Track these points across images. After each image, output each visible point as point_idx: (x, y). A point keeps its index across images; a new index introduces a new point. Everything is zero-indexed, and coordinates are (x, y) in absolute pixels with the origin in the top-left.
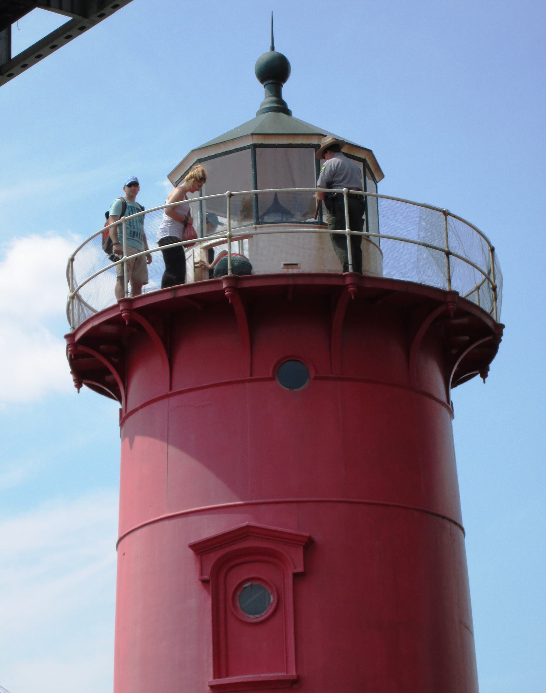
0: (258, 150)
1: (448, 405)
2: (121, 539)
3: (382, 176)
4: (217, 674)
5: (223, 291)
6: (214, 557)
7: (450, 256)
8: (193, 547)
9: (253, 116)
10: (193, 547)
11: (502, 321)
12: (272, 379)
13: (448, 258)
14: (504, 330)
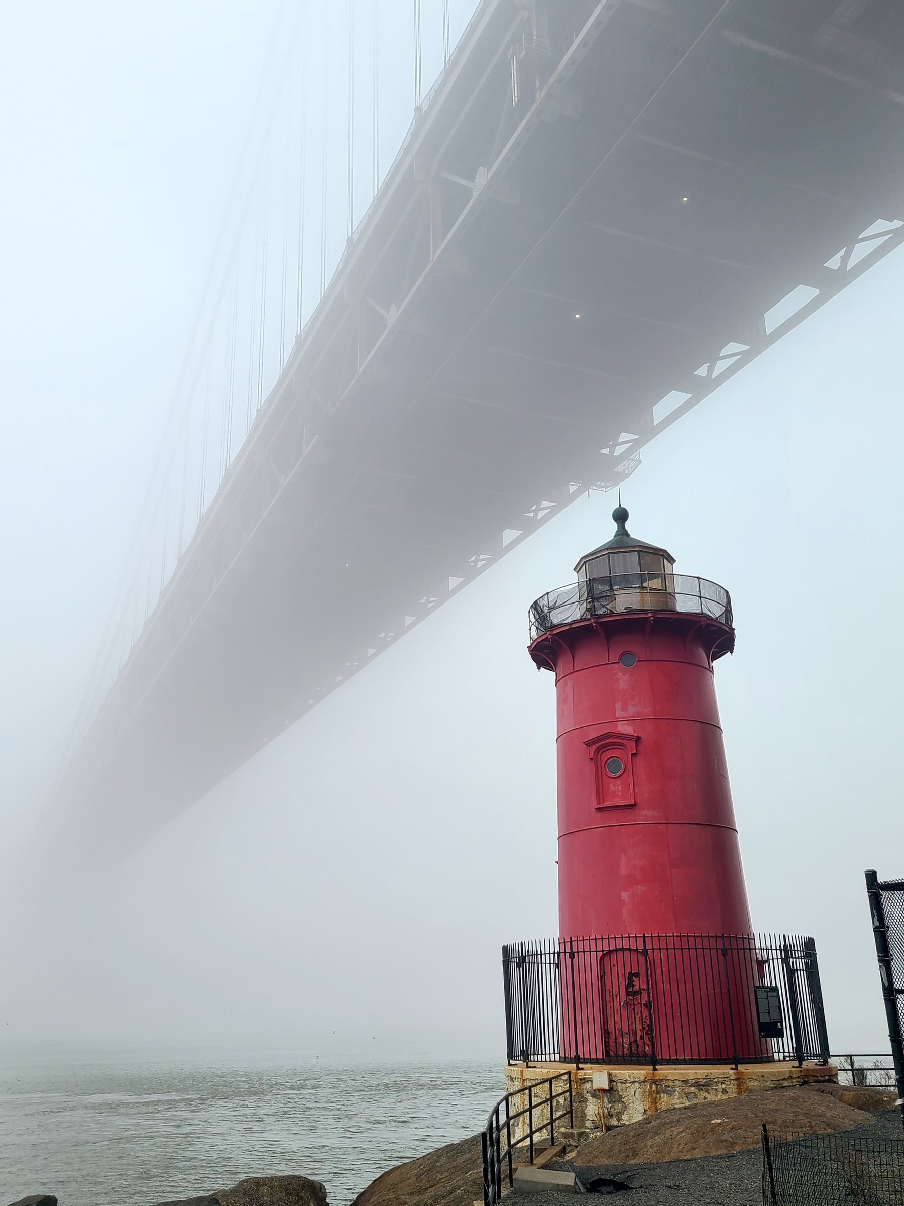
3: (675, 561)
4: (598, 802)
6: (594, 747)
9: (613, 538)
11: (734, 627)
12: (618, 663)
13: (700, 599)
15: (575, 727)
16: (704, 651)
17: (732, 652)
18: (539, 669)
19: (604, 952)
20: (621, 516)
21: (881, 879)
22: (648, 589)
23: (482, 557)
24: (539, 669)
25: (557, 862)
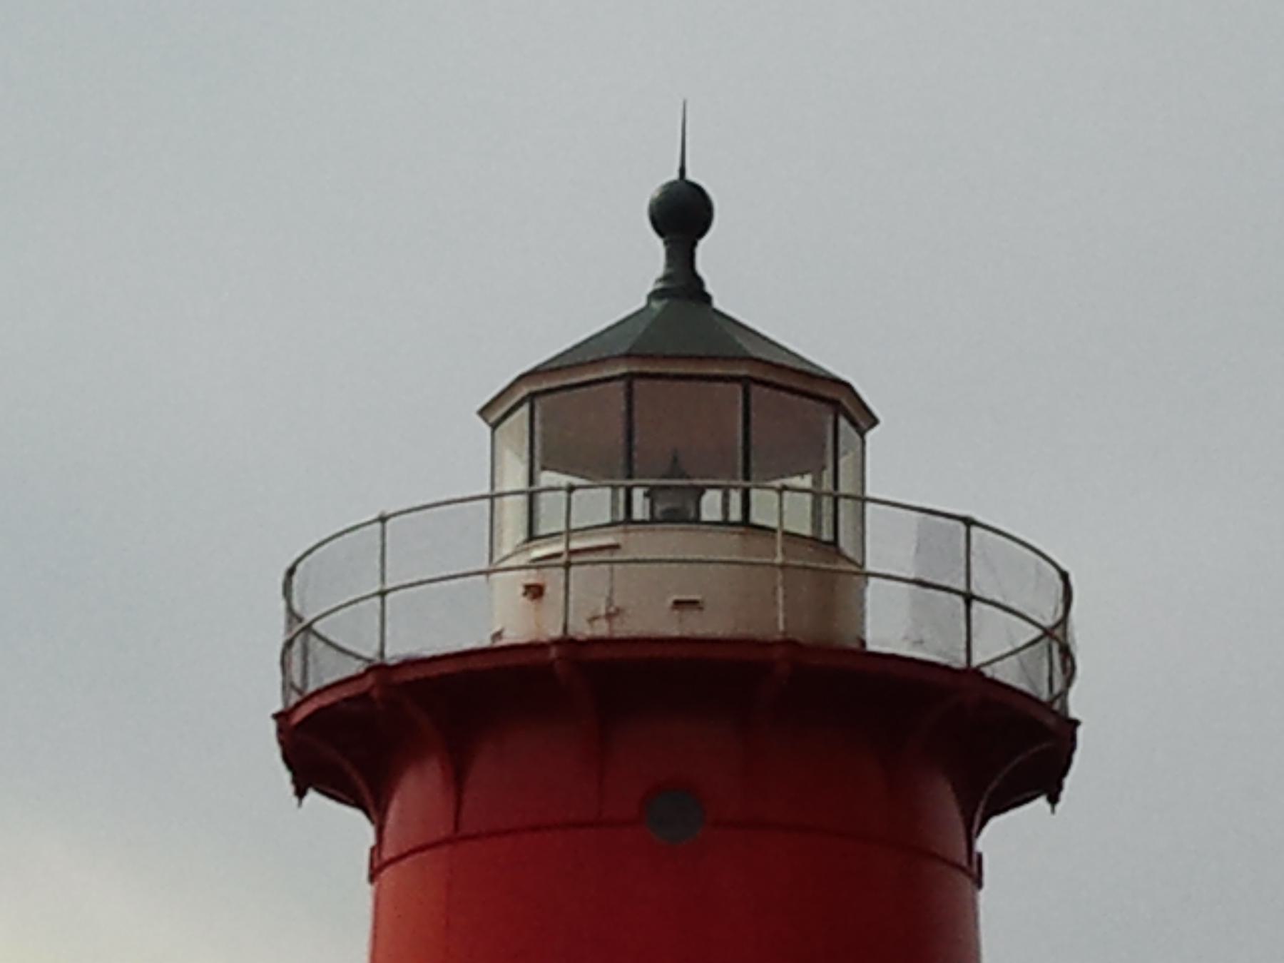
0: (639, 385)
3: (874, 422)
7: (976, 605)
11: (1074, 713)
14: (1081, 732)
16: (955, 790)
18: (300, 793)
22: (779, 535)
24: (300, 793)
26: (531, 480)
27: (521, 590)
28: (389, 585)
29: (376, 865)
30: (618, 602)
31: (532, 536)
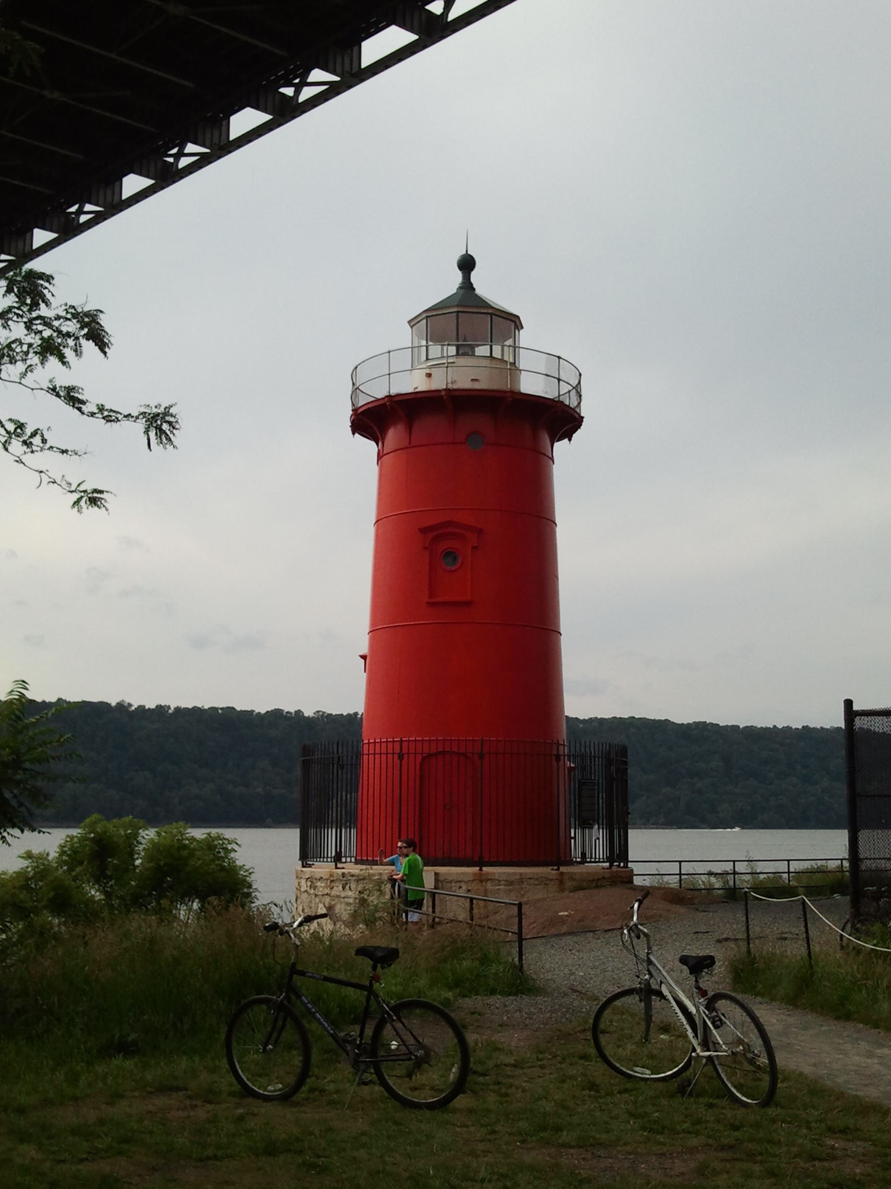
0: (460, 314)
1: (872, 943)
2: (376, 522)
3: (522, 328)
4: (431, 596)
5: (442, 396)
7: (561, 382)
8: (420, 530)
10: (420, 530)
11: (582, 415)
14: (584, 420)
15: (407, 510)
17: (570, 440)
18: (354, 434)
19: (424, 755)
20: (467, 264)
21: (856, 707)
23: (88, 207)
25: (364, 657)
26: (427, 343)
27: (425, 375)
28: (391, 372)
29: (381, 455)
30: (454, 379)
31: (427, 359)
